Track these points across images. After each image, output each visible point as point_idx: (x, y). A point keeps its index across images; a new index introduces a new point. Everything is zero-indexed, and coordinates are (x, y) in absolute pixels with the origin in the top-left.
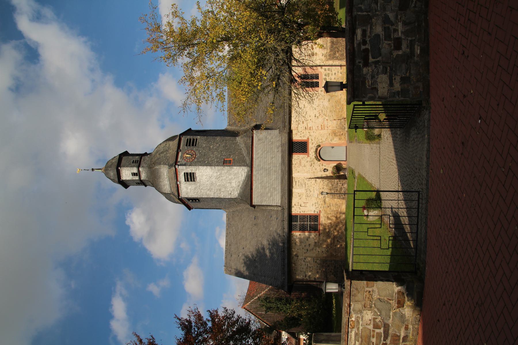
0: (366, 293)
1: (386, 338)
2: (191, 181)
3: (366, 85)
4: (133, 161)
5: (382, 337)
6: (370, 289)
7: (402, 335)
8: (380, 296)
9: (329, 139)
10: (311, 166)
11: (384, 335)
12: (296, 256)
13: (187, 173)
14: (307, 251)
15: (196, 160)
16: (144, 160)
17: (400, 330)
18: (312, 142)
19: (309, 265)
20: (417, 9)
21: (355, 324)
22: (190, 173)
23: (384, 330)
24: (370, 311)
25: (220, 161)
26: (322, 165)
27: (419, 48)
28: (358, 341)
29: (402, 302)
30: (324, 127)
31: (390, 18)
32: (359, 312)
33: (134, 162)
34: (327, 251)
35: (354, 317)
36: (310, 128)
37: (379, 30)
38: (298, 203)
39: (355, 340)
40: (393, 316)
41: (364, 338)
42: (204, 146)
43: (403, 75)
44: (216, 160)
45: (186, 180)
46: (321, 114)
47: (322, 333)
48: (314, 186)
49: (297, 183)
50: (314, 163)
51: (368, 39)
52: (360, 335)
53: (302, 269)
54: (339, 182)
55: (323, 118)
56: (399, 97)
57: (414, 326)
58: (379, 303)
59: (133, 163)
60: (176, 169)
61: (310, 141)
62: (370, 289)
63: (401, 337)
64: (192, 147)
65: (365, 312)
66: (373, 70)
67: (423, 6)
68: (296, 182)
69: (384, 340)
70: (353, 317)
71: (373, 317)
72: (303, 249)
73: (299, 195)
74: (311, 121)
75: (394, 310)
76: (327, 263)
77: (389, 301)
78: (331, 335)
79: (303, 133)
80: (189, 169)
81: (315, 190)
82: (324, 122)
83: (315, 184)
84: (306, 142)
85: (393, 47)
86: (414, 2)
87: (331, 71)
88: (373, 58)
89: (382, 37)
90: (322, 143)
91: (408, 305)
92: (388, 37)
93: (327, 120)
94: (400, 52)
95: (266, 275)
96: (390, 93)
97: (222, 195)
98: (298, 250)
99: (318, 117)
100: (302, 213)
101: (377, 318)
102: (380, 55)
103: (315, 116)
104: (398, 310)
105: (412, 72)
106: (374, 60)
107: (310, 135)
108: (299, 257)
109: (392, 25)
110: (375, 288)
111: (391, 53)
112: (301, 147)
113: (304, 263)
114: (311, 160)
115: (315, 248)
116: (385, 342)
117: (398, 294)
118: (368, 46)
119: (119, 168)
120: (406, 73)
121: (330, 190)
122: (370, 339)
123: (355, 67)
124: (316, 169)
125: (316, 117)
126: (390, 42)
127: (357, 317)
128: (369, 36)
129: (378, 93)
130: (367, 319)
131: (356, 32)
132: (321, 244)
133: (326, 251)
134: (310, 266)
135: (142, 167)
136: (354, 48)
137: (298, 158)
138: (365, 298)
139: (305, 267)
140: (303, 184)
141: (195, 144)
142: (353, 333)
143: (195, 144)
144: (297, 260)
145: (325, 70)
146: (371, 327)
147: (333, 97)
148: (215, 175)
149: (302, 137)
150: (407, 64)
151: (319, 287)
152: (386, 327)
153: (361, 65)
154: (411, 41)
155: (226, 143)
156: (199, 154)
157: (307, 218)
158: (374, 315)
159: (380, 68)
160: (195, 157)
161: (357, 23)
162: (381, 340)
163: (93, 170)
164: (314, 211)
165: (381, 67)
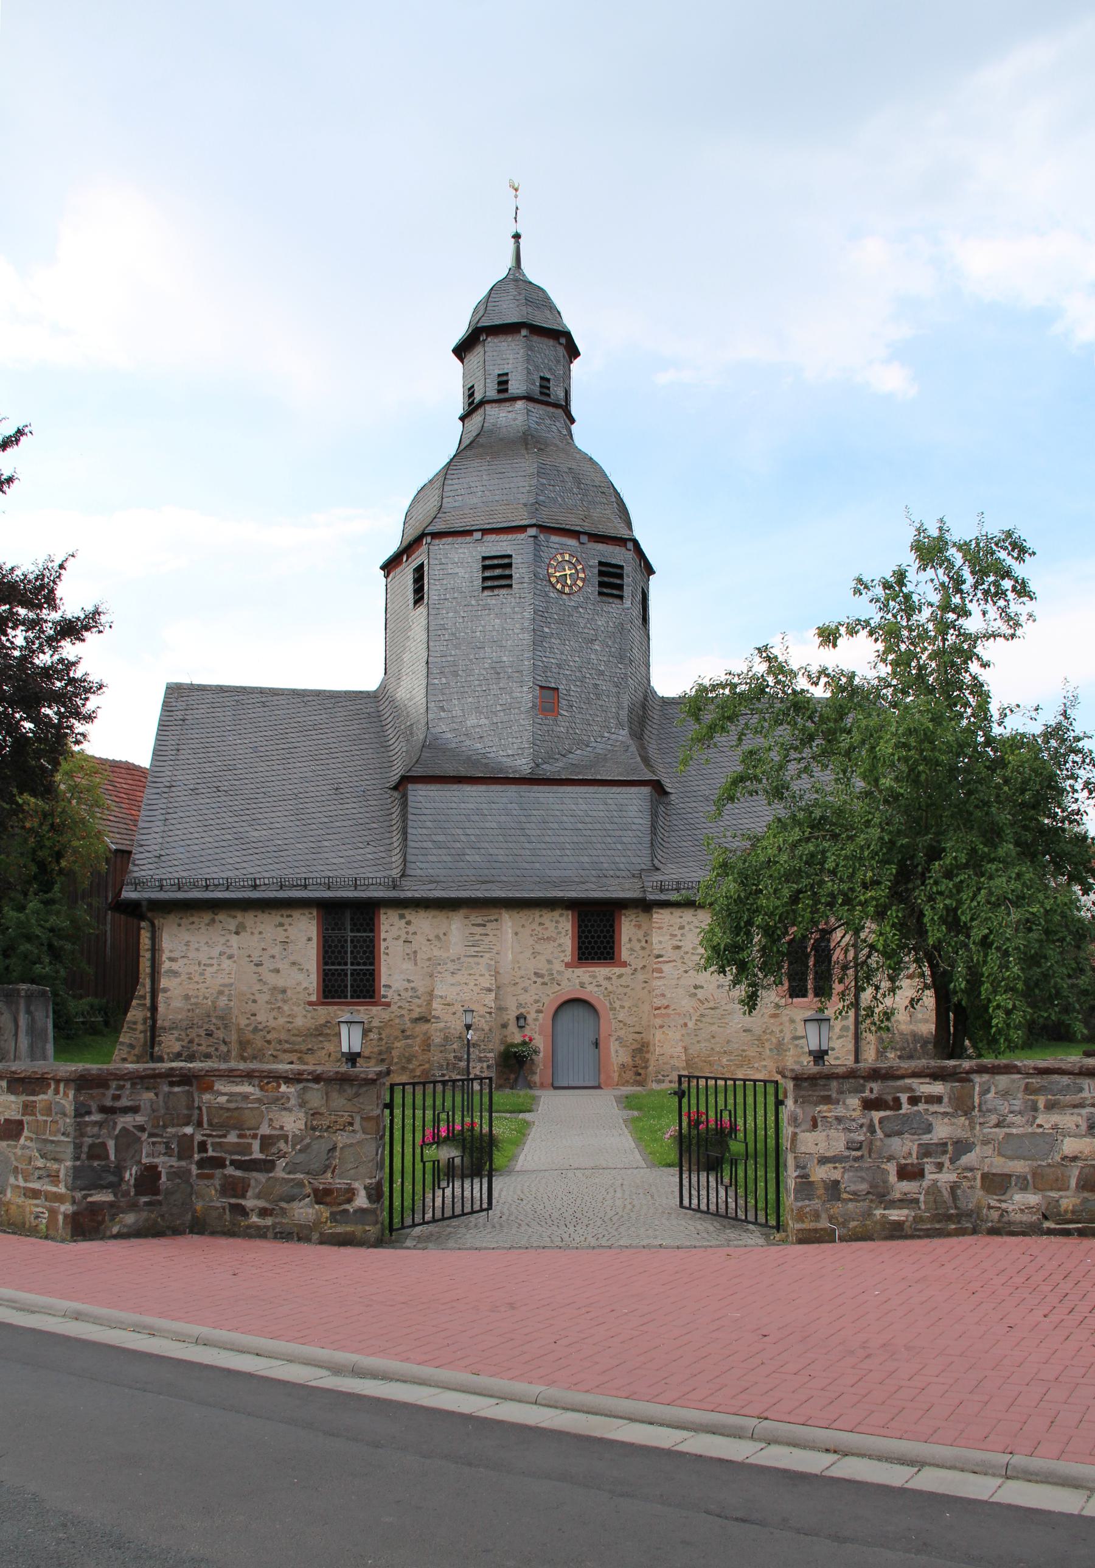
0: (349, 1116)
1: (238, 1165)
2: (485, 579)
3: (821, 1106)
4: (548, 380)
6: (357, 1126)
7: (249, 1203)
8: (342, 1148)
9: (623, 1032)
10: (535, 973)
11: (245, 1161)
12: (237, 927)
14: (257, 965)
15: (552, 595)
16: (552, 417)
17: (258, 1197)
18: (614, 977)
19: (209, 969)
20: (985, 1211)
21: (271, 1094)
22: (510, 577)
23: (260, 1160)
24: (303, 1127)
25: (549, 674)
26: (539, 1011)
27: (902, 1218)
28: (228, 1101)
29: (328, 1199)
30: (662, 1016)
31: (965, 1154)
32: (300, 1100)
33: (545, 383)
34: (256, 1030)
35: (289, 1090)
36: (660, 971)
37: (942, 1131)
38: (415, 933)
39: (231, 1095)
40: (293, 1180)
41: (236, 1114)
42: (599, 623)
43: (843, 1186)
44: (552, 660)
45: (487, 562)
46: (705, 1006)
47: (51, 1015)
48: (472, 983)
49: (479, 930)
51: (921, 1107)
52: (245, 1106)
53: (197, 946)
54: (485, 1065)
55: (692, 1011)
56: (797, 1177)
57: (271, 1230)
58: (325, 1146)
59: (542, 378)
60: (522, 529)
61: (617, 970)
62: (357, 1126)
63: (243, 1202)
64: (596, 580)
65: (301, 1115)
66: (854, 1120)
67: (990, 1224)
68: (484, 926)
69: (233, 1162)
70: (288, 1087)
72: (263, 949)
73: (441, 936)
75: (310, 1183)
76: (218, 1029)
77: (330, 1171)
78: (46, 1041)
79: (643, 948)
80: (520, 571)
81: (459, 988)
83: (477, 989)
84: (612, 958)
85: (903, 1161)
86: (999, 1205)
87: (840, 1037)
88: (881, 1121)
89: (926, 1139)
90: (611, 1009)
91: (322, 1214)
92: (926, 1151)
93: (686, 1025)
94: (893, 1178)
95: (171, 827)
96: (805, 1157)
97: (436, 681)
98: (260, 933)
99: (695, 994)
100: (383, 945)
101: (286, 1142)
102: (888, 1136)
103: (696, 987)
104: (308, 1190)
105: (851, 1205)
106: (876, 1122)
107: (635, 970)
108: (236, 937)
109: (950, 1159)
110: (360, 1136)
111: (890, 1158)
112: (596, 942)
113: (215, 953)
115: (265, 989)
116: (228, 1163)
117: (348, 1189)
118: (906, 1108)
119: (524, 332)
120: (848, 1193)
121: (460, 1038)
122: (235, 1128)
123: (862, 1081)
125: (694, 991)
126: (914, 1156)
128: (928, 1110)
129: (803, 1131)
130: (284, 1120)
131: (938, 1083)
132: (279, 1008)
133: (256, 1027)
134: (208, 975)
135: (528, 411)
136: (902, 1077)
137: (560, 933)
138: (335, 1115)
139: (203, 957)
140: (477, 949)
141: (605, 590)
143: (605, 590)
144: (224, 929)
146: (265, 1130)
147: (756, 1042)
148: (505, 659)
149: (628, 946)
150: (868, 1193)
151: (134, 1002)
152: (267, 1166)
153: (867, 1094)
154: (917, 1201)
156: (573, 604)
157: (365, 964)
158: (295, 1136)
159: (859, 1135)
160: (563, 593)
161: (957, 1084)
162: (231, 1153)
163: (517, 237)
164: (389, 986)
165: (862, 1138)
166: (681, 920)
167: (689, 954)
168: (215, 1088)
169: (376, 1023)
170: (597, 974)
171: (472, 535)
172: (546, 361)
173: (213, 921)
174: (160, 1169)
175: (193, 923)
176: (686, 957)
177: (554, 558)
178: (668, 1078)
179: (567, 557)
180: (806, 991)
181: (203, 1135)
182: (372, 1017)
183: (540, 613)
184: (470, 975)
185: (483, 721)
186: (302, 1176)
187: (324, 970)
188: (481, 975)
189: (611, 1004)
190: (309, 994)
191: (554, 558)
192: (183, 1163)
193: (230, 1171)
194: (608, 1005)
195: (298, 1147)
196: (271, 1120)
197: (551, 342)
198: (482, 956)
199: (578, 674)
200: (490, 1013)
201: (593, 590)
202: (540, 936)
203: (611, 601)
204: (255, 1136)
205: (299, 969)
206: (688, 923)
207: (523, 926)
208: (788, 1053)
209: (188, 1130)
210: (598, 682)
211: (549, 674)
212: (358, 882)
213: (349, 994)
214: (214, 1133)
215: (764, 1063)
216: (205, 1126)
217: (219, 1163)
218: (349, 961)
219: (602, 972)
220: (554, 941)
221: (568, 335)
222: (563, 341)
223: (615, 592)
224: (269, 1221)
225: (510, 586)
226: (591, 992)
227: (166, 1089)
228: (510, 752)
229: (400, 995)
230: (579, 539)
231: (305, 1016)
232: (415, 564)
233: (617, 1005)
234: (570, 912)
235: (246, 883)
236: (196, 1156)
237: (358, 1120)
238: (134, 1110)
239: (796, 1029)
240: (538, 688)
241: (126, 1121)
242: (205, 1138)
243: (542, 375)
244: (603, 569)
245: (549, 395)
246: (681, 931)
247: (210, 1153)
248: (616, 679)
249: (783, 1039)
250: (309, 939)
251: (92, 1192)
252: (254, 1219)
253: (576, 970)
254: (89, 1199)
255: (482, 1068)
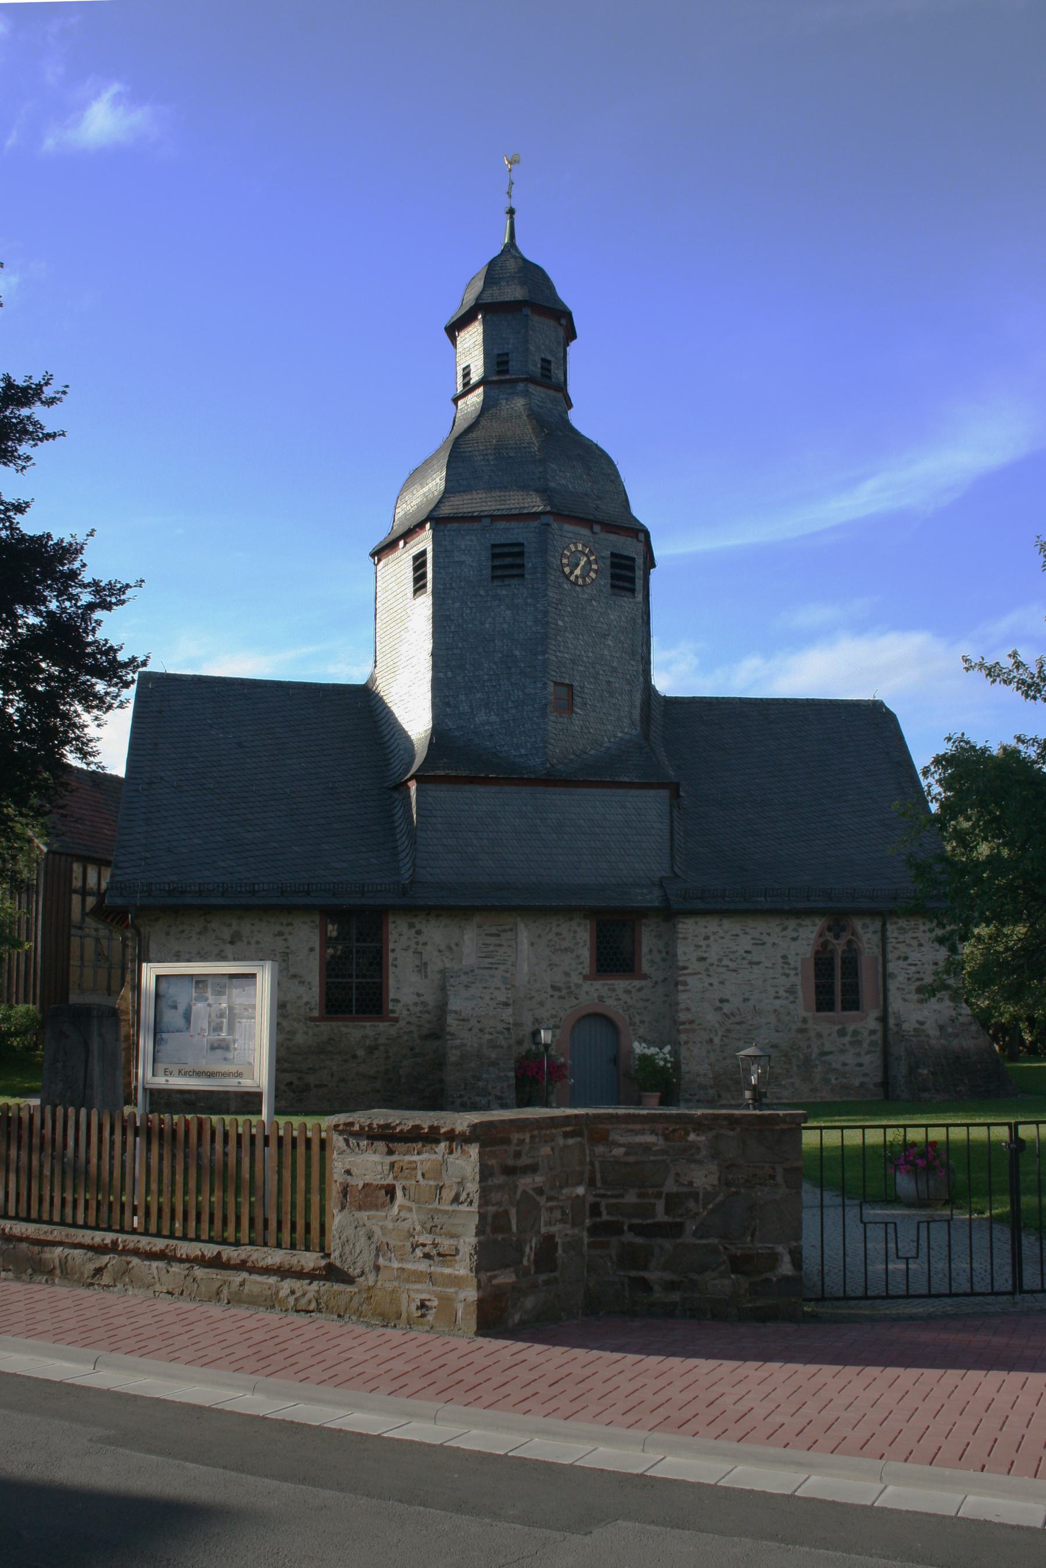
2: (494, 568)
4: (549, 362)
5: (641, 1221)
6: (780, 1179)
7: (653, 1275)
13: (521, 554)
15: (566, 586)
22: (522, 566)
24: (716, 1182)
25: (563, 670)
28: (626, 1154)
35: (699, 1139)
36: (685, 984)
38: (425, 944)
42: (612, 617)
44: (566, 656)
45: (497, 551)
46: (730, 1021)
49: (493, 940)
50: (561, 998)
55: (717, 1026)
59: (544, 360)
61: (637, 983)
62: (780, 1179)
63: (646, 1275)
64: (608, 572)
65: (714, 1168)
68: (498, 935)
69: (632, 1227)
70: (698, 1135)
71: (702, 1190)
73: (453, 946)
74: (706, 985)
75: (725, 1248)
82: (705, 1030)
87: (868, 1052)
90: (631, 1024)
93: (711, 1041)
99: (721, 1009)
100: (391, 956)
101: (697, 1201)
103: (722, 1001)
107: (656, 983)
108: (228, 946)
114: (573, 988)
116: (626, 1228)
124: (541, 1004)
125: (718, 1004)
127: (699, 1149)
140: (490, 960)
141: (617, 583)
142: (650, 1139)
143: (617, 583)
144: (217, 938)
145: (873, 1032)
146: (670, 1186)
147: (783, 1058)
152: (674, 1230)
155: (621, 694)
156: (586, 596)
163: (511, 212)
164: (397, 1001)
166: (706, 930)
167: (715, 967)
168: (610, 1138)
169: (382, 1040)
170: (617, 987)
171: (480, 521)
172: (547, 342)
173: (206, 929)
174: (557, 1239)
175: (183, 931)
176: (711, 969)
177: (567, 548)
178: (697, 1097)
179: (580, 548)
180: (833, 1004)
181: (596, 1196)
182: (379, 1034)
183: (554, 605)
184: (485, 988)
185: (493, 718)
186: (716, 1241)
187: (327, 983)
188: (498, 989)
189: (630, 1018)
190: (311, 1009)
191: (567, 548)
192: (576, 1231)
193: (629, 1237)
194: (627, 1019)
195: (711, 1206)
196: (678, 1174)
197: (552, 323)
198: (496, 969)
199: (591, 670)
200: (508, 1029)
201: (606, 582)
202: (557, 947)
203: (623, 594)
204: (658, 1196)
205: (300, 982)
206: (714, 933)
207: (539, 936)
208: (816, 1070)
209: (580, 1190)
210: (611, 679)
211: (563, 670)
212: (366, 889)
213: (354, 1008)
214: (609, 1193)
215: (791, 1080)
216: (599, 1184)
217: (614, 1229)
218: (354, 973)
219: (621, 984)
220: (571, 952)
221: (568, 315)
222: (564, 322)
223: (626, 585)
224: (676, 1297)
225: (522, 576)
226: (612, 1006)
227: (561, 1141)
228: (523, 751)
229: (408, 1010)
230: (591, 529)
231: (306, 1033)
232: (415, 551)
233: (637, 1019)
234: (588, 922)
235: (243, 889)
236: (587, 1221)
237: (779, 1170)
238: (533, 1169)
239: (823, 1044)
240: (552, 684)
241: (526, 1182)
242: (598, 1199)
243: (543, 356)
244: (616, 560)
245: (550, 378)
246: (706, 942)
247: (605, 1217)
248: (628, 677)
249: (811, 1055)
250: (312, 950)
251: (496, 1272)
252: (658, 1295)
253: (594, 983)
254: (495, 1282)
255: (502, 1088)
